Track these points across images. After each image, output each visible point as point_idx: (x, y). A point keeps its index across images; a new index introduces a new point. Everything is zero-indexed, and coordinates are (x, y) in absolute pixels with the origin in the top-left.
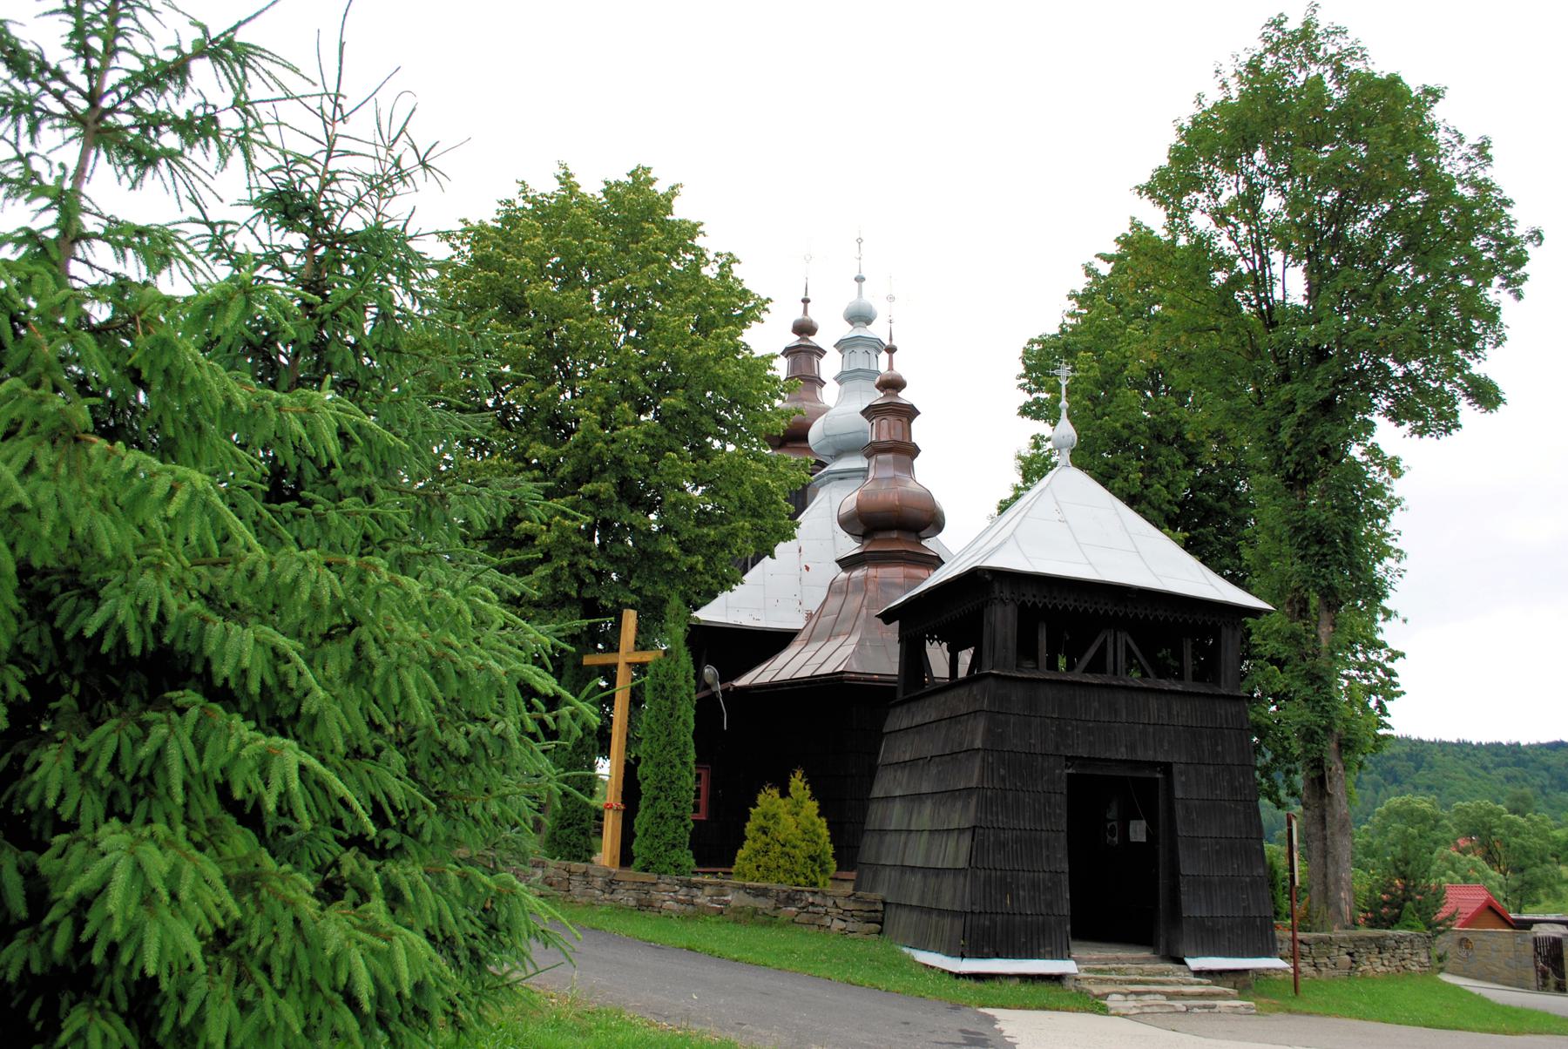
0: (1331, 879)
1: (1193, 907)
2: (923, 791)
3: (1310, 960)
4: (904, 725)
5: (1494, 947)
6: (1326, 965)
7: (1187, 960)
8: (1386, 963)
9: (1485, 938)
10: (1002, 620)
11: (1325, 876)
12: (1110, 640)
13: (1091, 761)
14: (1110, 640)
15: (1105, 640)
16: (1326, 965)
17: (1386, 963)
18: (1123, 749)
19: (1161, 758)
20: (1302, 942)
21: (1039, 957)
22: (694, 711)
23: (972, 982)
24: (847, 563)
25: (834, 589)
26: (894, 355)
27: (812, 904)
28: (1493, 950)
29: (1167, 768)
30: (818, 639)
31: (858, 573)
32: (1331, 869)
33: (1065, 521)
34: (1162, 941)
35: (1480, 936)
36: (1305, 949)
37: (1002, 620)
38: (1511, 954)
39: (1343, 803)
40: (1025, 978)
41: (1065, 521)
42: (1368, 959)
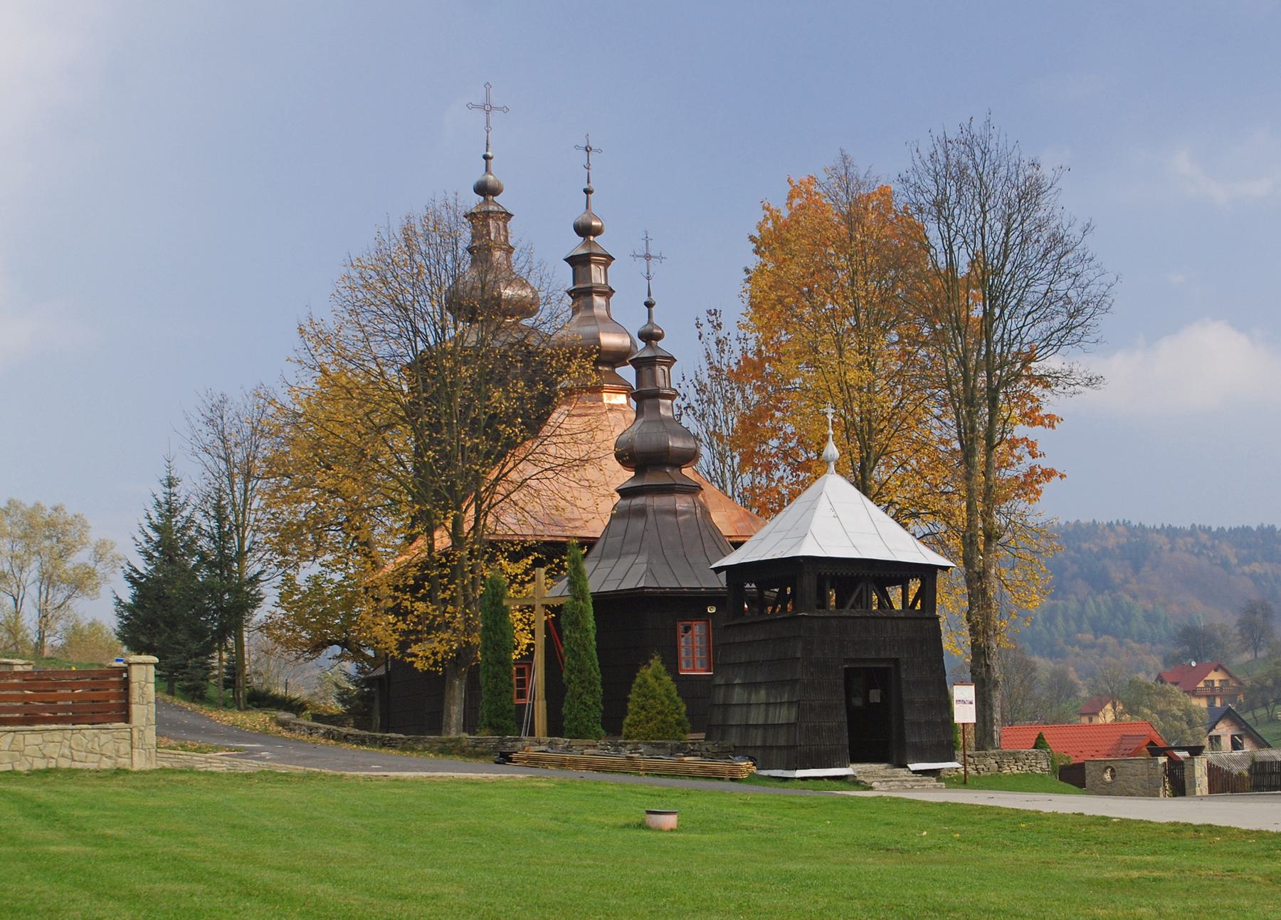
0: (988, 718)
1: (912, 739)
2: (759, 681)
3: (974, 767)
4: (738, 640)
5: (1133, 771)
6: (983, 770)
7: (909, 765)
8: (1020, 768)
9: (1125, 764)
10: (808, 583)
11: (984, 717)
12: (864, 589)
13: (854, 661)
14: (864, 589)
15: (862, 589)
16: (983, 770)
17: (1020, 768)
18: (873, 653)
19: (893, 656)
20: (969, 756)
21: (834, 767)
22: (1206, 778)
23: (801, 782)
24: (625, 493)
25: (618, 515)
26: (653, 309)
27: (693, 750)
28: (1131, 775)
29: (896, 661)
30: (608, 557)
31: (638, 501)
32: (988, 713)
33: (588, 169)
34: (895, 758)
35: (1121, 763)
36: (971, 760)
37: (808, 583)
38: (1145, 777)
39: (996, 670)
40: (829, 778)
41: (588, 169)
42: (1008, 766)
